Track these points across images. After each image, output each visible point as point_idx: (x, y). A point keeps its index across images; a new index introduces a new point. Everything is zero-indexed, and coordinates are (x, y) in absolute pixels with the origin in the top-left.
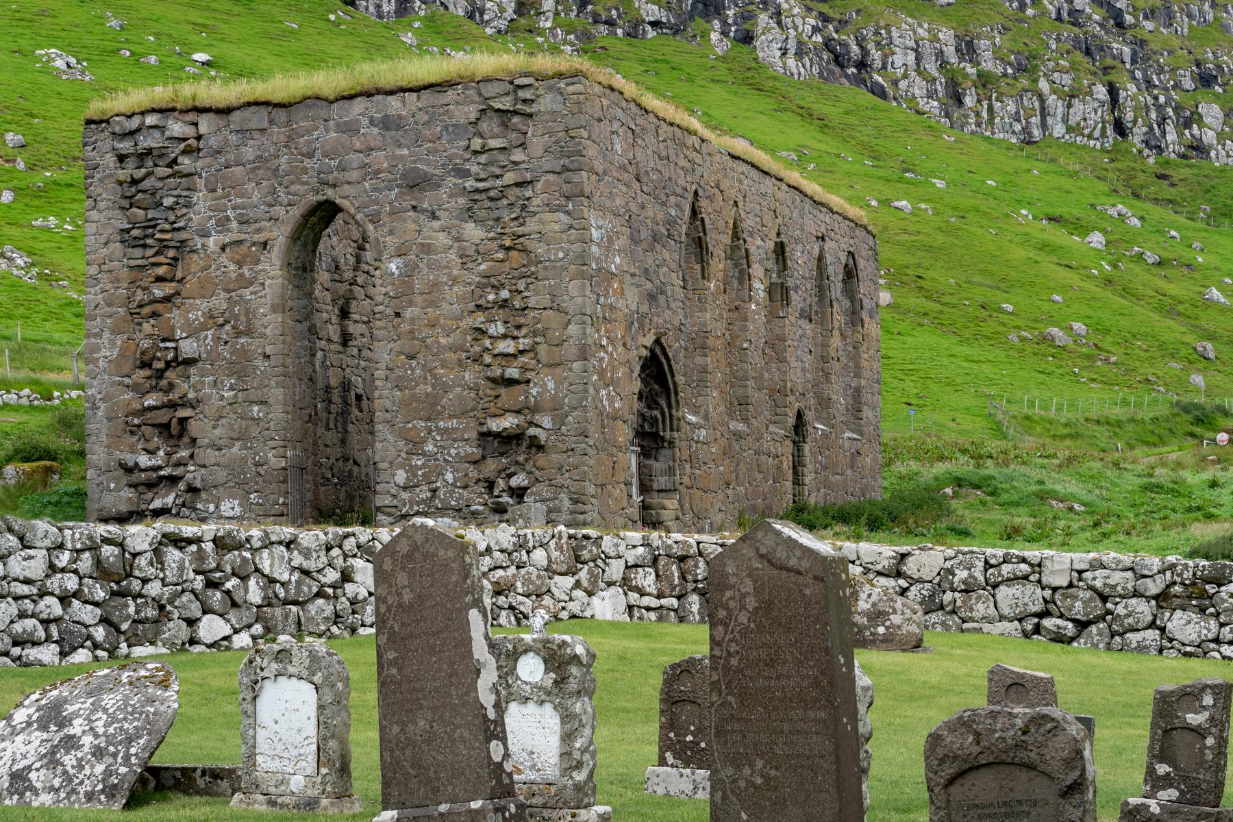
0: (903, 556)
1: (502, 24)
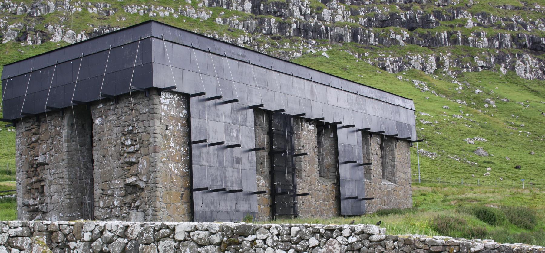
0: (127, 227)
1: (432, 71)
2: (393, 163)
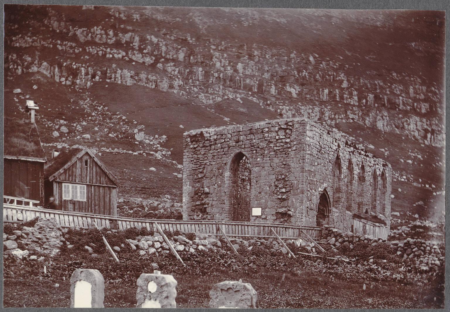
2: (384, 202)
